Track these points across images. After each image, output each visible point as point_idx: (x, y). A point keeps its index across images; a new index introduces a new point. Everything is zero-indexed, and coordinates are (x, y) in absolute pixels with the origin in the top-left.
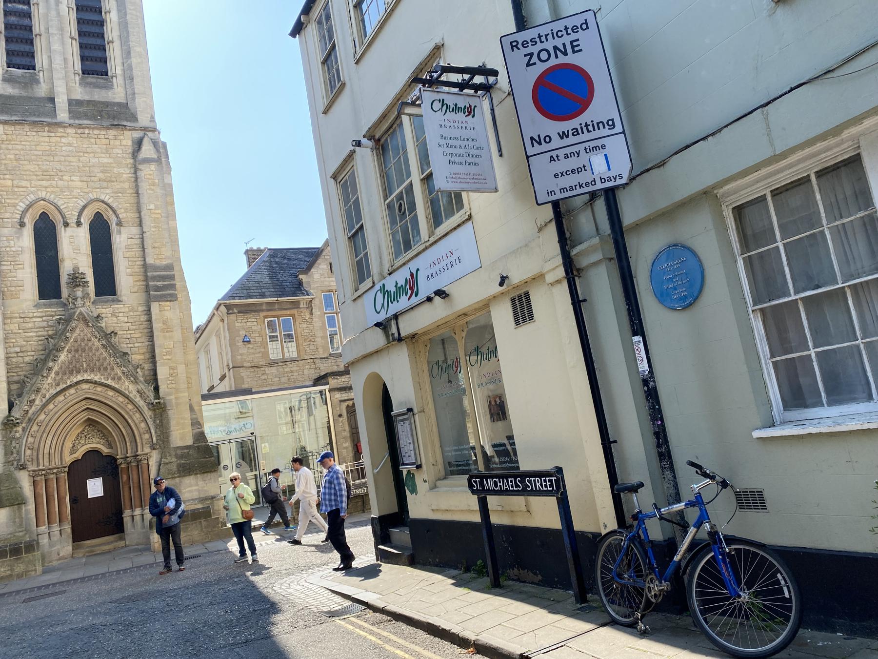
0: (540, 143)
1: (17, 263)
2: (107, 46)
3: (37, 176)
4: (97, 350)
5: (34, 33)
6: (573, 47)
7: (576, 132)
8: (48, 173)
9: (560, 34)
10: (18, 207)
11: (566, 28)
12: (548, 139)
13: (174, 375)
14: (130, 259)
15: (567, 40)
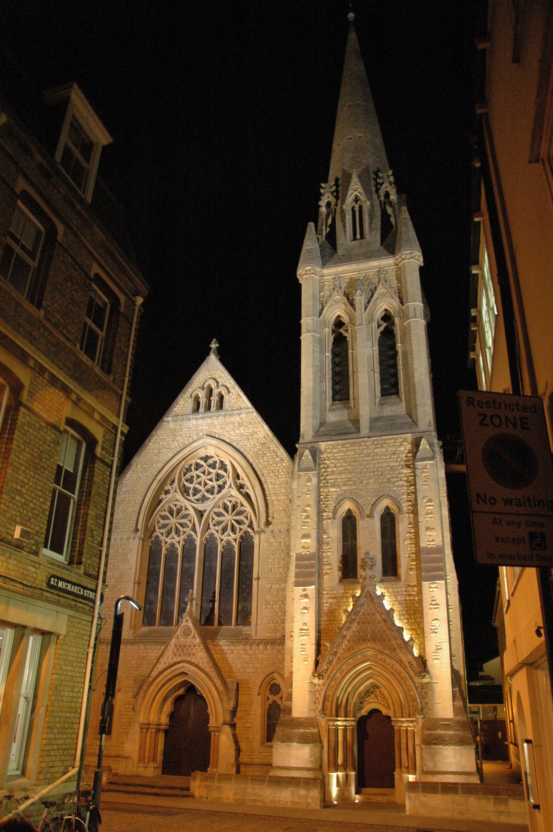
0: (485, 502)
4: (379, 623)
11: (517, 404)
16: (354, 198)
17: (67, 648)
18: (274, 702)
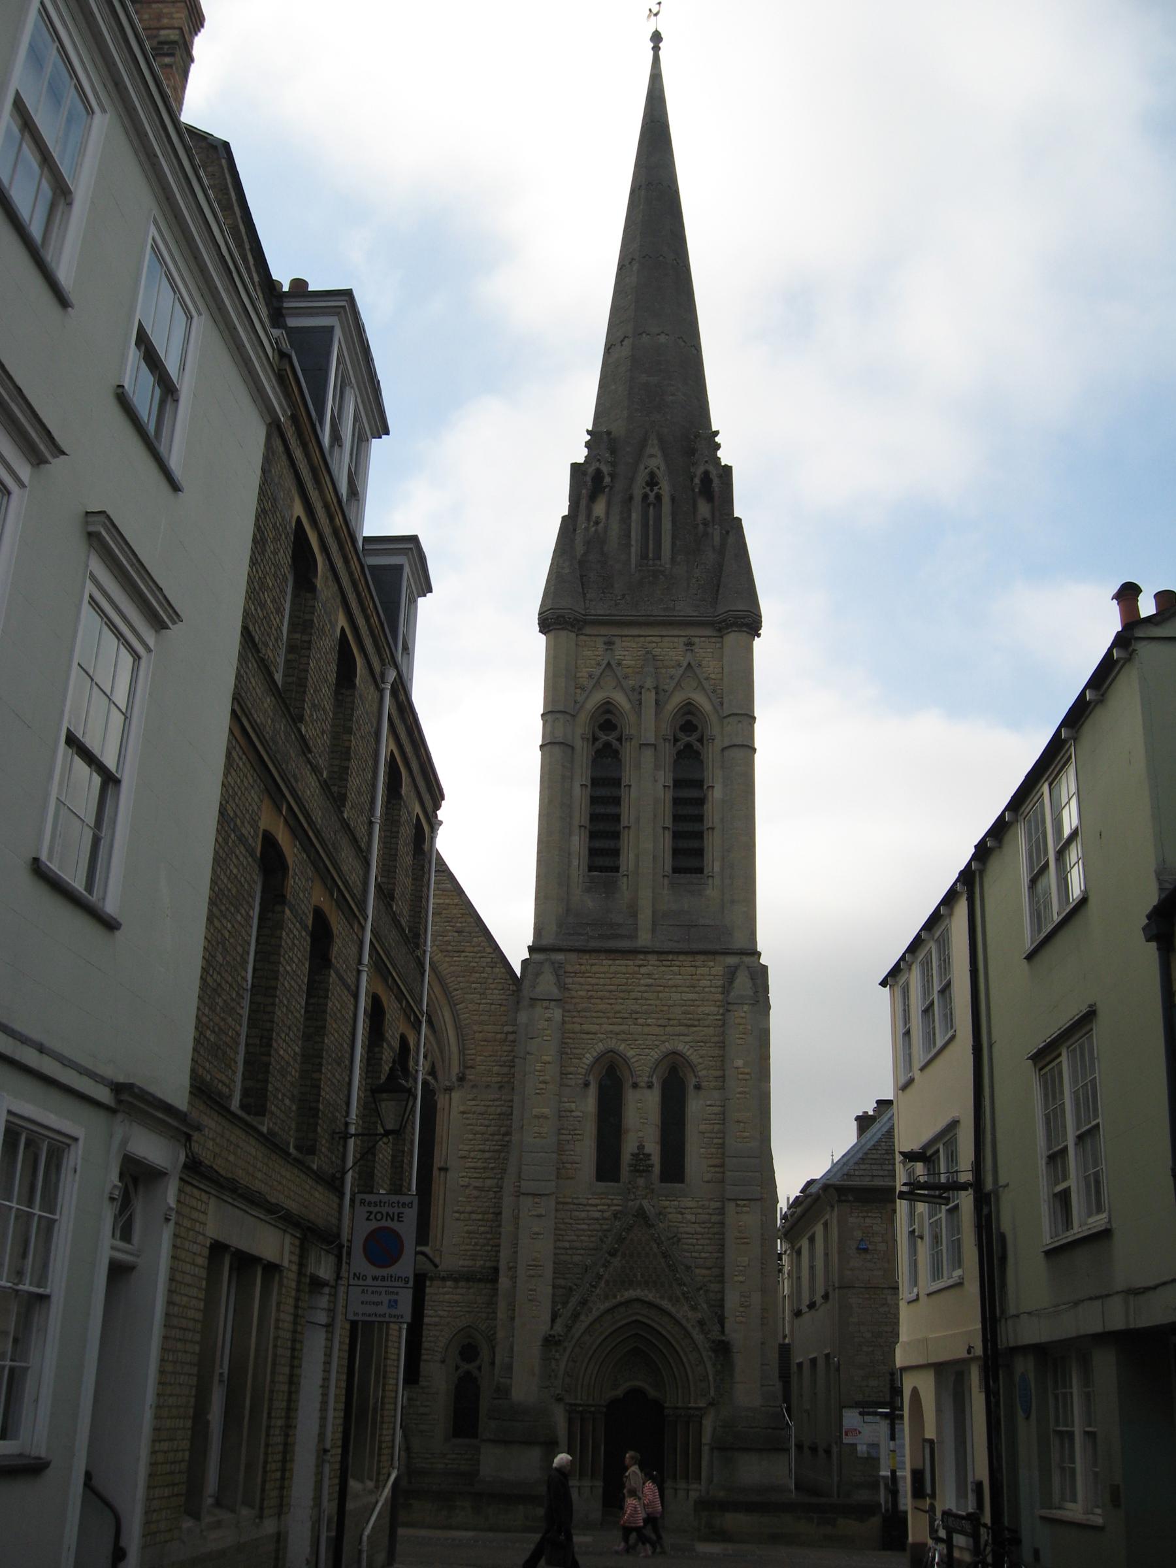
0: (359, 1279)
1: (577, 1132)
2: (705, 833)
3: (608, 1018)
5: (622, 826)
6: (399, 1217)
7: (383, 1279)
8: (621, 1015)
9: (394, 1205)
10: (585, 1060)
11: (398, 1203)
12: (365, 1278)
13: (746, 1304)
14: (706, 1135)
15: (396, 1210)
16: (647, 478)
17: (222, 1024)
18: (468, 1373)
